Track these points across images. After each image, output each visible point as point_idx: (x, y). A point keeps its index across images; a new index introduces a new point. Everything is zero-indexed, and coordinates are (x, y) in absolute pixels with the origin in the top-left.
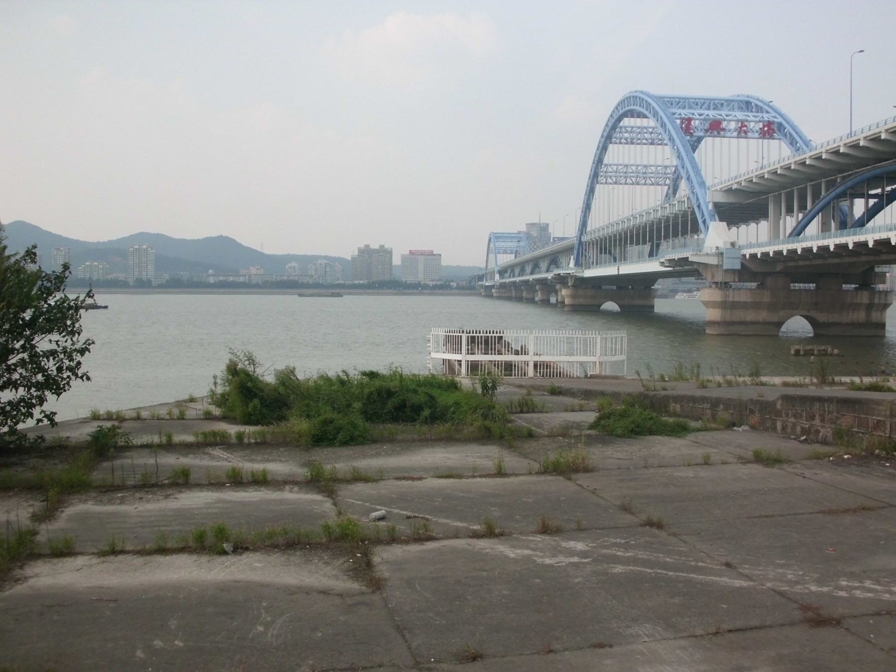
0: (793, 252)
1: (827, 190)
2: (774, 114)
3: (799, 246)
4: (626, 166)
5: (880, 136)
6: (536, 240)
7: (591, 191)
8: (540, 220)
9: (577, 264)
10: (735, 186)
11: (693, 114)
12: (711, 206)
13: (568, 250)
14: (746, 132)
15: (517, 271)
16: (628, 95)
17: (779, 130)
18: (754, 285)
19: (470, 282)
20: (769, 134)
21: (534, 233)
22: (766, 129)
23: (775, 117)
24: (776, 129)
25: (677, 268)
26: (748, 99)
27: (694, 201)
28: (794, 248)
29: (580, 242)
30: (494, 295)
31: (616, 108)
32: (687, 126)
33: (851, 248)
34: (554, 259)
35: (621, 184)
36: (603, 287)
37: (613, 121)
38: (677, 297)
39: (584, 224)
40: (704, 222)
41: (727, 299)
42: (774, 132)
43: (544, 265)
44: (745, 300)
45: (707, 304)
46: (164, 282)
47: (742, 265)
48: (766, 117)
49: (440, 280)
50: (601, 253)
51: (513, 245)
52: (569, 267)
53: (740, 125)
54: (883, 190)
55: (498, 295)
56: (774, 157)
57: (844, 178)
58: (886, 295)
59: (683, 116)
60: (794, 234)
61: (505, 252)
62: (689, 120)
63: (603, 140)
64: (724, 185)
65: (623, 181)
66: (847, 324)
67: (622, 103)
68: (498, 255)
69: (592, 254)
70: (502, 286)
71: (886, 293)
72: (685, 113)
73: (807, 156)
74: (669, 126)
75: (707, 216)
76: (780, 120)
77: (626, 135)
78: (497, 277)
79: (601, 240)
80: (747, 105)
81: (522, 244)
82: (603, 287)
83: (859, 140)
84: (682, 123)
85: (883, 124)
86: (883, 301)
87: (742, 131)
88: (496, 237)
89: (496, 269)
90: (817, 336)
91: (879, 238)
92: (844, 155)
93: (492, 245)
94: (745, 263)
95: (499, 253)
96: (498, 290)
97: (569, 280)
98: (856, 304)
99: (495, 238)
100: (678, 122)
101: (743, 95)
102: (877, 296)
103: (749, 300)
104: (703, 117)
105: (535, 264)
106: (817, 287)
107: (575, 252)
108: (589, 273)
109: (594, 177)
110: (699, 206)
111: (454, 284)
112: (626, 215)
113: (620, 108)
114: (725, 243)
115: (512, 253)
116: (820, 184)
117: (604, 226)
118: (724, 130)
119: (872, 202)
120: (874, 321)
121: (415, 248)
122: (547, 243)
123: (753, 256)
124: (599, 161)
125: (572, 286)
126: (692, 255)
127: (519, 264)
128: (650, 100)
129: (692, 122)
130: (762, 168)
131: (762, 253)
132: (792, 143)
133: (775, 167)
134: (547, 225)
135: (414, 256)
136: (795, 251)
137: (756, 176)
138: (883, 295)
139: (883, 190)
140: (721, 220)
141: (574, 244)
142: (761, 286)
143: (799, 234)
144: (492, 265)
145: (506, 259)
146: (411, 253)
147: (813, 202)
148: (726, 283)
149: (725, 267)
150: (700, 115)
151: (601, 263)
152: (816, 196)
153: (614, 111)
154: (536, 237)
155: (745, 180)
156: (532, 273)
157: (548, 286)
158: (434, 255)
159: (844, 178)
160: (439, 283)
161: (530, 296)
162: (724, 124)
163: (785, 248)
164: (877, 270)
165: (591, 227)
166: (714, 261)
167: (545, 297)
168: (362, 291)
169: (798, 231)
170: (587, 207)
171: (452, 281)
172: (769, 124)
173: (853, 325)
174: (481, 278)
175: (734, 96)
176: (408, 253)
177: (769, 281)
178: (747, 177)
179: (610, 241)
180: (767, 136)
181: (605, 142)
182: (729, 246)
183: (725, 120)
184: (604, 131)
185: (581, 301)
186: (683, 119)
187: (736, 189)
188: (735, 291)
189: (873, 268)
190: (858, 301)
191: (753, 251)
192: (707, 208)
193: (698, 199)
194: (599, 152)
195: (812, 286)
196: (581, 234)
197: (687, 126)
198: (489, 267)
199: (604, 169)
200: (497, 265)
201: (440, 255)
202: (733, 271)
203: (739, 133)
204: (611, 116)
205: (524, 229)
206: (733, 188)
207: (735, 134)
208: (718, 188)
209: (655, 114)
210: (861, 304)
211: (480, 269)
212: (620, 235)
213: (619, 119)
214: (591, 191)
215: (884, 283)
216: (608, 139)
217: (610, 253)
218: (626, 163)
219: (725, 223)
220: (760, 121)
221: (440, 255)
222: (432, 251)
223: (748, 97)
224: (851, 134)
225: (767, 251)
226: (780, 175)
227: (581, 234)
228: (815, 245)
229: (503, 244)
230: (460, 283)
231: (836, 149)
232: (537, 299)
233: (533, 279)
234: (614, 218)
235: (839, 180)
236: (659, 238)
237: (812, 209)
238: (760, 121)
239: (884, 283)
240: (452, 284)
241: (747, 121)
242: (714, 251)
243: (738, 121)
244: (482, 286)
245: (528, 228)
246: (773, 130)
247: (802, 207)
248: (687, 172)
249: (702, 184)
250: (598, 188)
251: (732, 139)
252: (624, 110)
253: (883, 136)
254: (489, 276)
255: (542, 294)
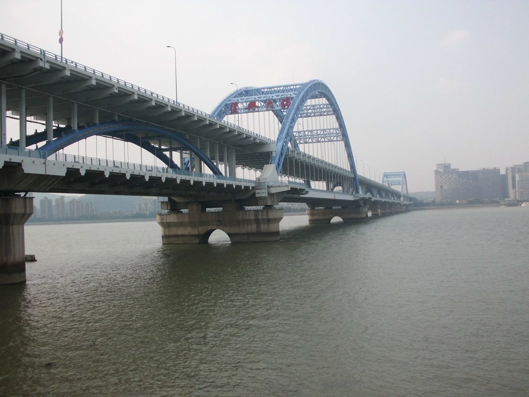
6: (442, 174)
8: (445, 162)
21: (441, 170)
28: (221, 183)
36: (340, 207)
38: (523, 205)
41: (163, 221)
44: (173, 221)
46: (292, 208)
66: (244, 234)
80: (247, 92)
90: (233, 243)
98: (246, 220)
103: (176, 221)
120: (263, 231)
134: (450, 164)
154: (442, 173)
168: (84, 221)
173: (248, 234)
188: (167, 215)
190: (247, 218)
195: (220, 209)
219: (25, 172)
251: (242, 114)
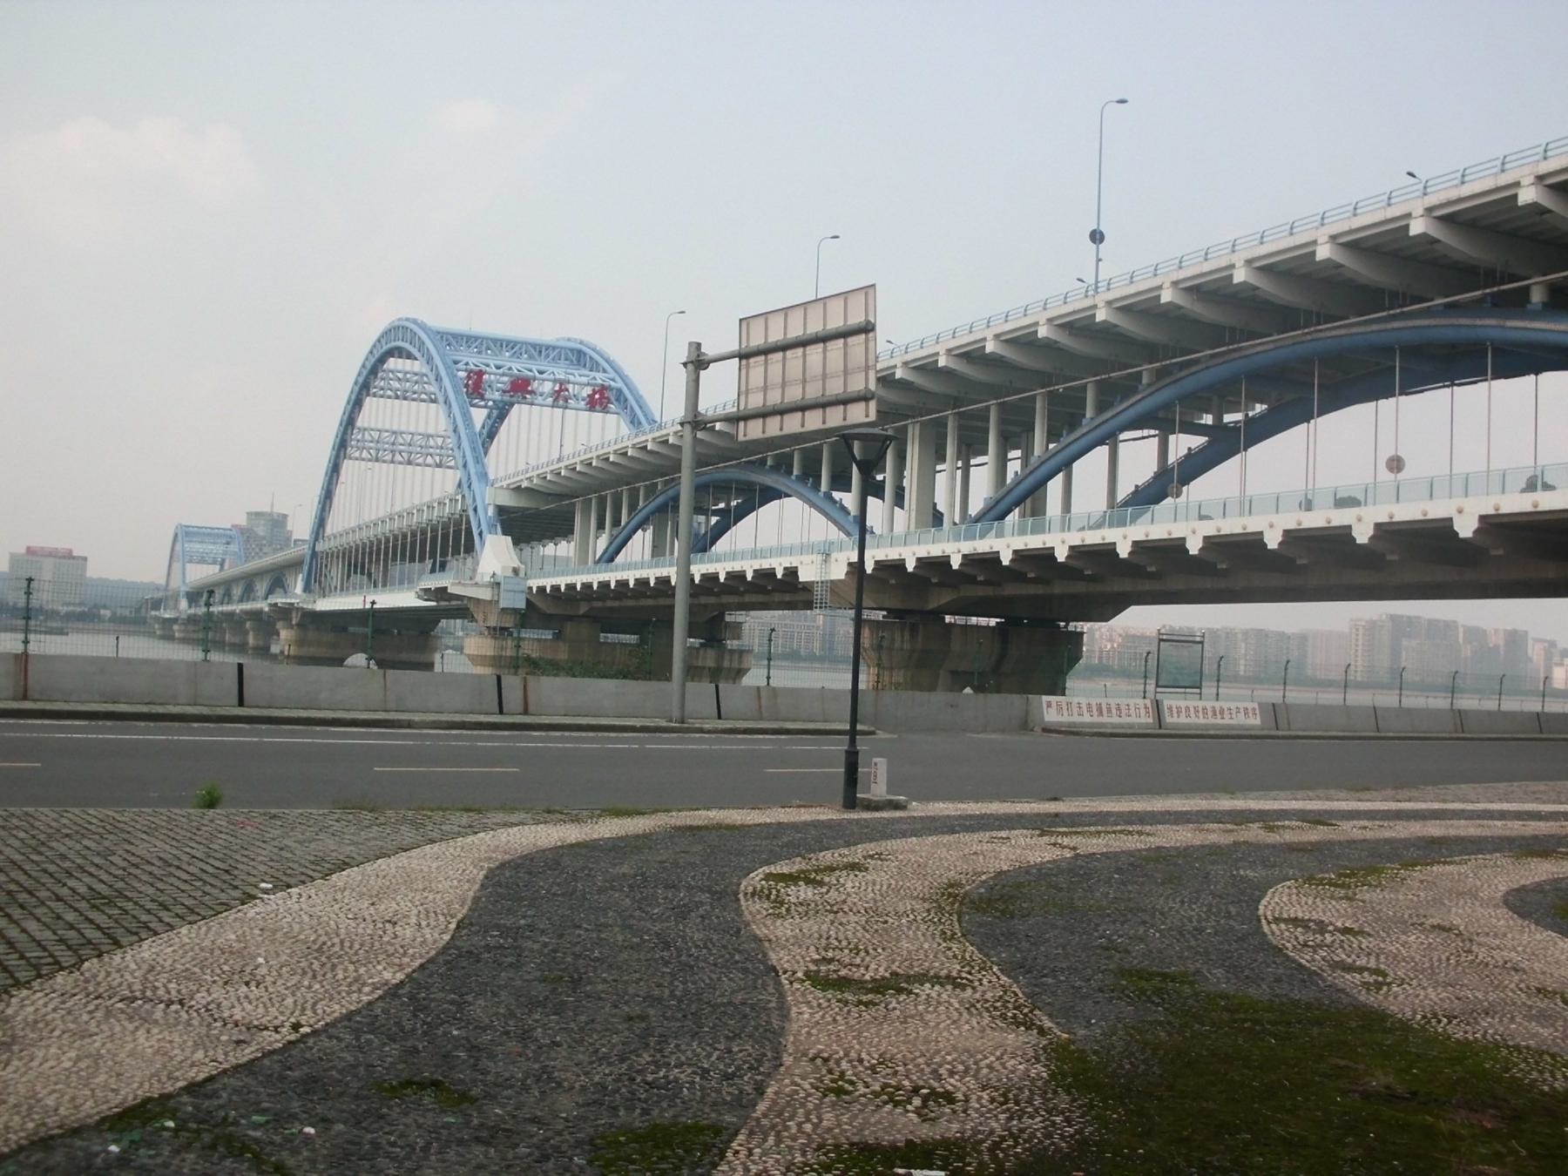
0: (604, 585)
1: (646, 498)
2: (612, 374)
3: (612, 577)
4: (394, 433)
5: (1159, 296)
7: (335, 470)
9: (307, 589)
10: (525, 484)
11: (488, 366)
12: (491, 511)
13: (295, 565)
14: (566, 400)
15: (237, 591)
16: (397, 323)
17: (617, 400)
18: (548, 635)
19: (138, 610)
20: (601, 404)
22: (597, 396)
23: (613, 380)
24: (613, 399)
25: (443, 603)
26: (579, 346)
27: (469, 501)
29: (314, 554)
30: (177, 635)
31: (379, 341)
32: (475, 386)
33: (749, 578)
34: (278, 578)
35: (384, 462)
36: (351, 629)
37: (373, 360)
39: (321, 523)
40: (480, 534)
42: (609, 402)
43: (261, 587)
45: (475, 660)
47: (528, 602)
48: (600, 378)
49: (80, 604)
50: (355, 572)
51: (217, 549)
52: (296, 593)
53: (557, 388)
54: (728, 504)
55: (182, 635)
56: (610, 435)
57: (666, 483)
58: (740, 657)
59: (472, 367)
60: (988, 516)
61: (202, 561)
62: (480, 374)
63: (357, 389)
64: (513, 480)
65: (389, 457)
67: (386, 334)
68: (188, 565)
69: (336, 572)
70: (192, 620)
71: (741, 653)
72: (473, 360)
73: (648, 438)
74: (446, 382)
75: (484, 527)
76: (620, 384)
77: (396, 385)
78: (184, 604)
79: (379, 541)
81: (233, 548)
82: (351, 629)
83: (1037, 324)
84: (469, 377)
85: (1201, 259)
86: (735, 665)
87: (560, 397)
88: (187, 534)
89: (184, 589)
91: (1023, 547)
92: (947, 373)
93: (178, 547)
94: (532, 599)
95: (191, 561)
96: (183, 628)
97: (294, 615)
98: (696, 667)
99: (185, 534)
100: (462, 374)
101: (575, 340)
102: (727, 657)
104: (501, 371)
105: (248, 582)
106: (642, 641)
107: (306, 568)
108: (325, 605)
109: (342, 447)
110: (475, 510)
111: (106, 613)
112: (352, 525)
113: (383, 342)
114: (504, 568)
115: (214, 563)
116: (638, 490)
117: (432, 502)
118: (532, 392)
119: (714, 520)
121: (38, 542)
122: (288, 546)
123: (542, 589)
124: (349, 422)
125: (298, 625)
126: (453, 584)
127: (242, 578)
128: (424, 337)
129: (486, 377)
130: (560, 460)
131: (583, 584)
132: (634, 422)
133: (624, 445)
135: (34, 558)
136: (715, 577)
137: (615, 452)
138: (736, 656)
139: (728, 504)
140: (505, 533)
141: (304, 555)
142: (558, 636)
143: (611, 560)
144: (176, 583)
145: (200, 573)
146: (30, 551)
147: (629, 514)
148: (502, 629)
149: (502, 604)
150: (498, 367)
151: (393, 584)
152: (633, 507)
153: (374, 346)
155: (598, 457)
156: (241, 601)
157: (266, 624)
158: (74, 558)
159: (1161, 374)
160: (78, 609)
161: (237, 640)
162: (535, 385)
163: (595, 579)
164: (728, 618)
165: (506, 470)
166: (485, 594)
167: (261, 643)
169: (610, 557)
170: (328, 496)
171: (105, 607)
172: (603, 389)
174: (156, 604)
175: (563, 339)
176: (23, 551)
177: (569, 628)
178: (601, 452)
179: (434, 539)
180: (597, 408)
181: (360, 393)
182: (510, 573)
183: (535, 379)
184: (359, 375)
185: (312, 651)
186: (471, 371)
187: (526, 488)
189: (722, 616)
191: (736, 566)
192: (486, 513)
193: (474, 500)
194: (349, 407)
196: (316, 539)
197: (475, 386)
198: (330, 529)
199: (357, 435)
200: (184, 582)
201: (85, 559)
202: (515, 611)
203: (555, 400)
204: (371, 352)
205: (242, 521)
206: (1412, 233)
207: (550, 400)
208: (505, 484)
209: (430, 360)
210: (704, 668)
211: (158, 588)
212: (405, 536)
213: (382, 360)
214: (335, 470)
215: (739, 637)
216: (364, 389)
217: (370, 575)
218: (395, 428)
220: (588, 384)
221: (85, 559)
222: (71, 551)
223: (581, 343)
224: (1097, 288)
225: (625, 578)
226: (651, 452)
227: (316, 539)
228: (631, 576)
229: (198, 546)
230: (119, 611)
231: (1224, 274)
232: (275, 649)
233: (242, 611)
234: (369, 515)
235: (1145, 380)
236: (444, 554)
237: (628, 523)
238: (588, 384)
239: (739, 637)
240: (102, 612)
241: (569, 382)
242: (487, 579)
243: (555, 381)
244: (157, 618)
245: (248, 519)
246: (608, 398)
247: (616, 522)
248: (464, 457)
249: (484, 476)
250: (347, 467)
252: (389, 346)
253: (899, 374)
254: (171, 603)
255: (256, 637)
